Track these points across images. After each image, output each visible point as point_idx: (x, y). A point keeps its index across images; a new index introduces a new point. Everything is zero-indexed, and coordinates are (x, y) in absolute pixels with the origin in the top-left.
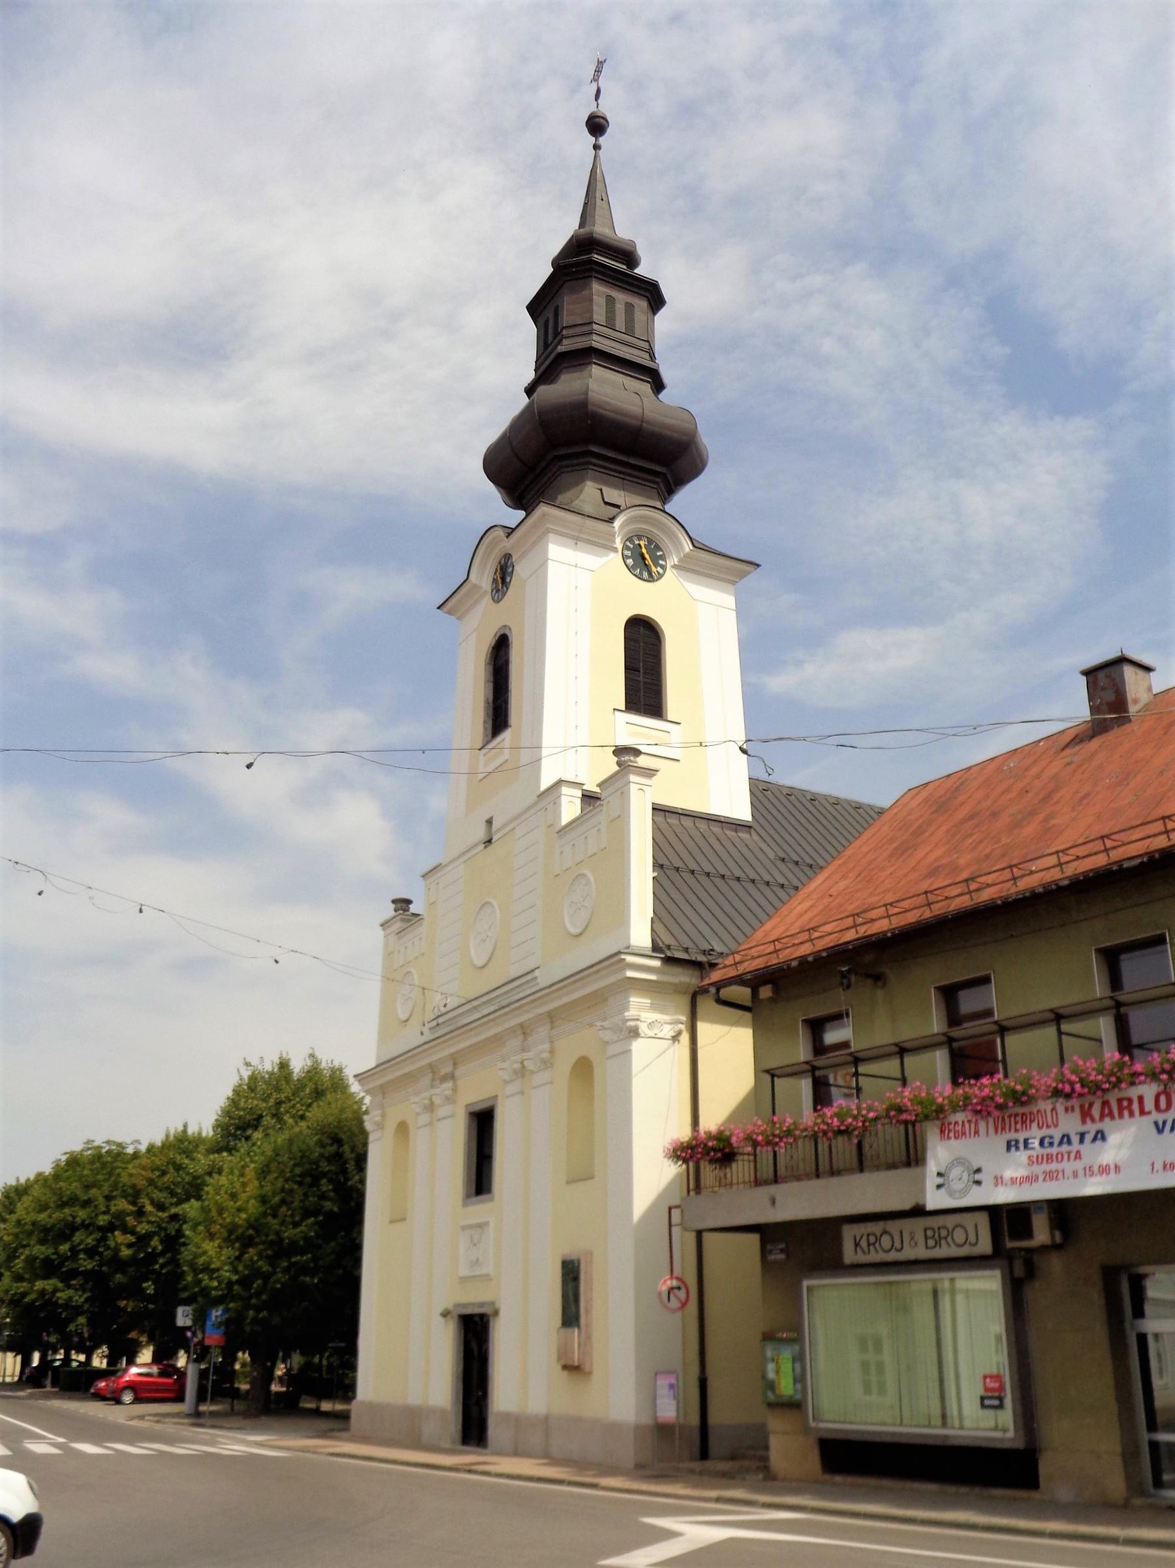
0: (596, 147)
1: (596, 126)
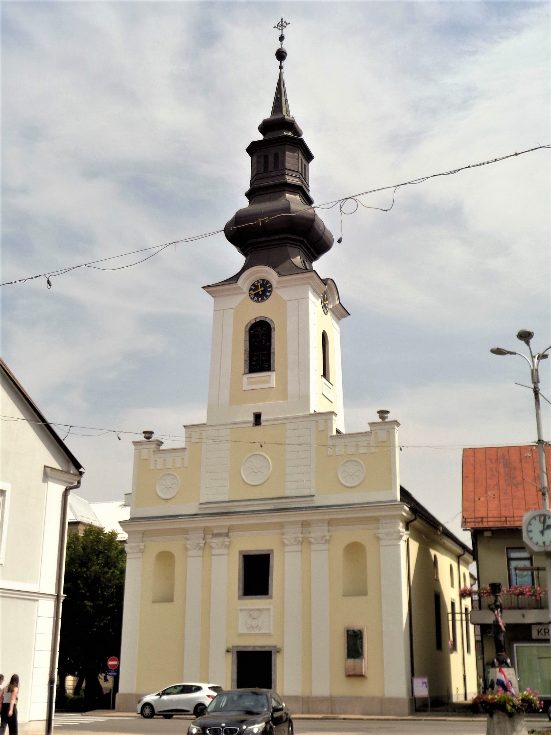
0: (281, 67)
1: (281, 55)
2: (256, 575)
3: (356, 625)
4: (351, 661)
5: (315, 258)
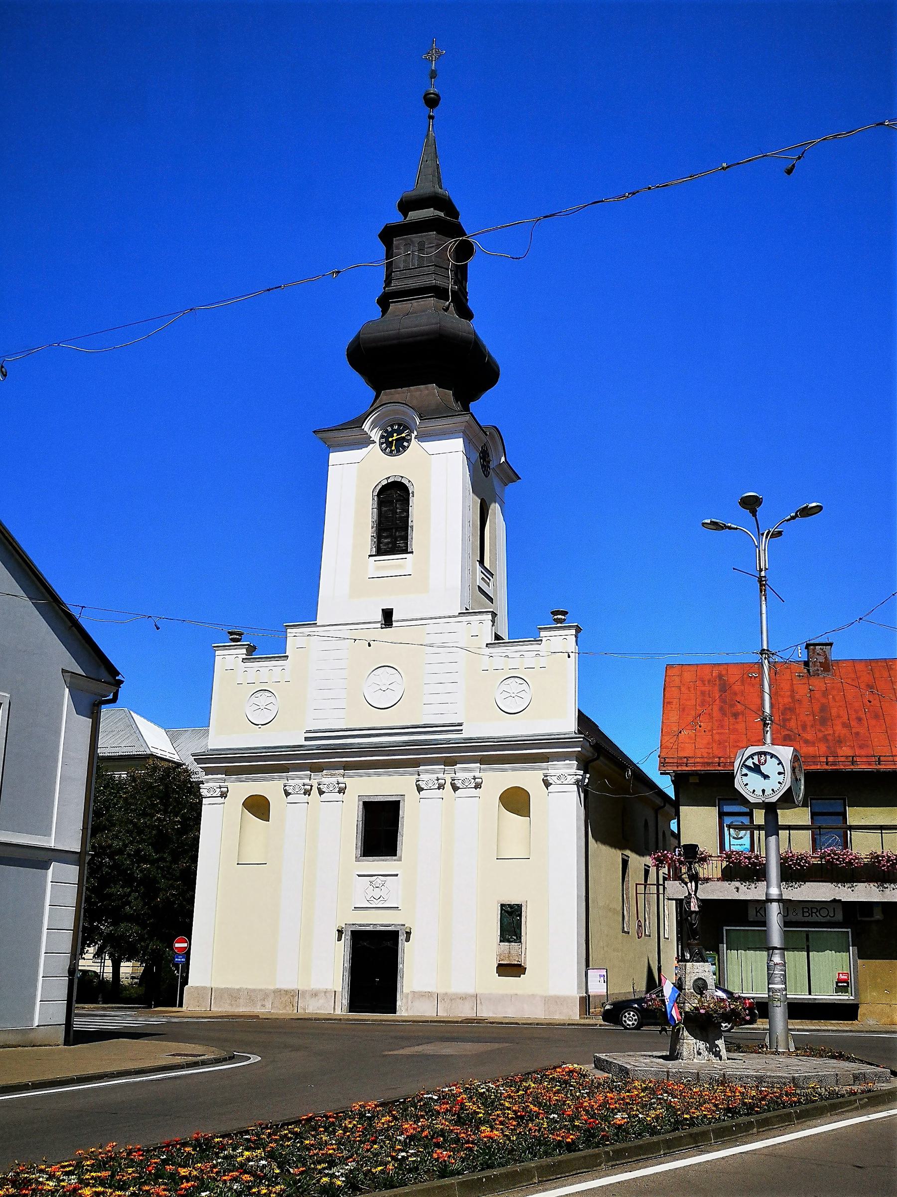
2: (380, 830)
5: (475, 397)
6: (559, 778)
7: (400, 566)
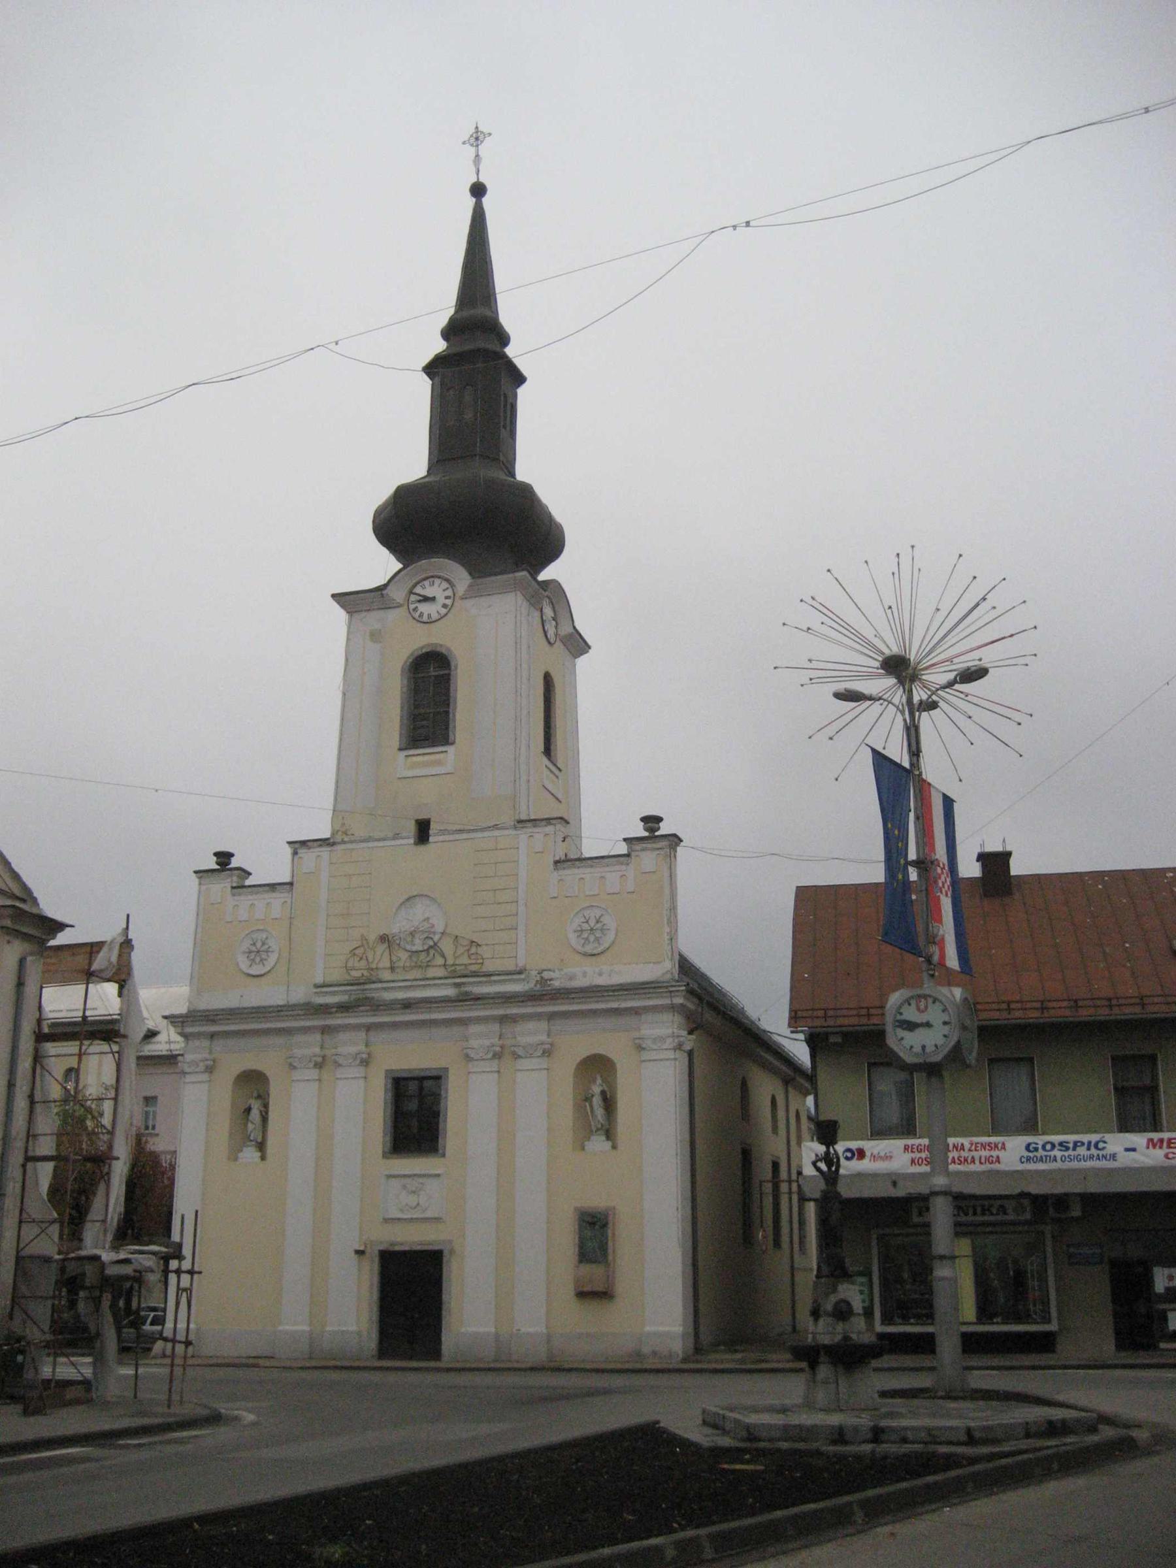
2: (415, 1119)
3: (596, 1201)
4: (586, 1269)
6: (655, 1040)
7: (439, 763)
